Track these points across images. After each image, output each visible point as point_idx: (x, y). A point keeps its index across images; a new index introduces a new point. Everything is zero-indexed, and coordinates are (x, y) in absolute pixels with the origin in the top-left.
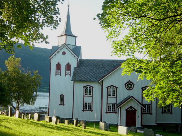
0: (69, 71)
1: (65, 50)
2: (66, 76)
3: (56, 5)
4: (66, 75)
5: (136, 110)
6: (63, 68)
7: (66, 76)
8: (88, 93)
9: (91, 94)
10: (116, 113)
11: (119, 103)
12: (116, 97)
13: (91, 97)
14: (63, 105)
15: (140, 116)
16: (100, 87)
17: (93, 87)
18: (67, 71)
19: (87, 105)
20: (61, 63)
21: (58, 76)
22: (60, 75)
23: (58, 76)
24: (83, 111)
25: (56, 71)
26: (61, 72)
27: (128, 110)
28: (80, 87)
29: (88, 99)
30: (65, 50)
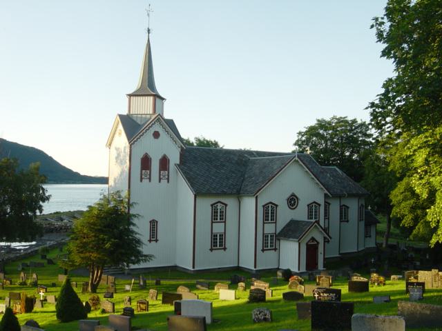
0: (148, 171)
1: (157, 128)
2: (160, 182)
3: (377, 102)
4: (160, 179)
5: (318, 243)
6: (155, 165)
7: (160, 182)
8: (270, 218)
9: (223, 219)
10: (275, 249)
11: (280, 229)
12: (276, 223)
13: (224, 224)
14: (157, 241)
15: (323, 253)
16: (238, 204)
17: (226, 205)
18: (144, 171)
19: (217, 239)
20: (151, 155)
21: (146, 181)
22: (150, 181)
23: (146, 181)
24: (211, 250)
25: (141, 172)
26: (150, 175)
27: (309, 243)
28: (206, 204)
29: (218, 228)
30: (157, 128)
